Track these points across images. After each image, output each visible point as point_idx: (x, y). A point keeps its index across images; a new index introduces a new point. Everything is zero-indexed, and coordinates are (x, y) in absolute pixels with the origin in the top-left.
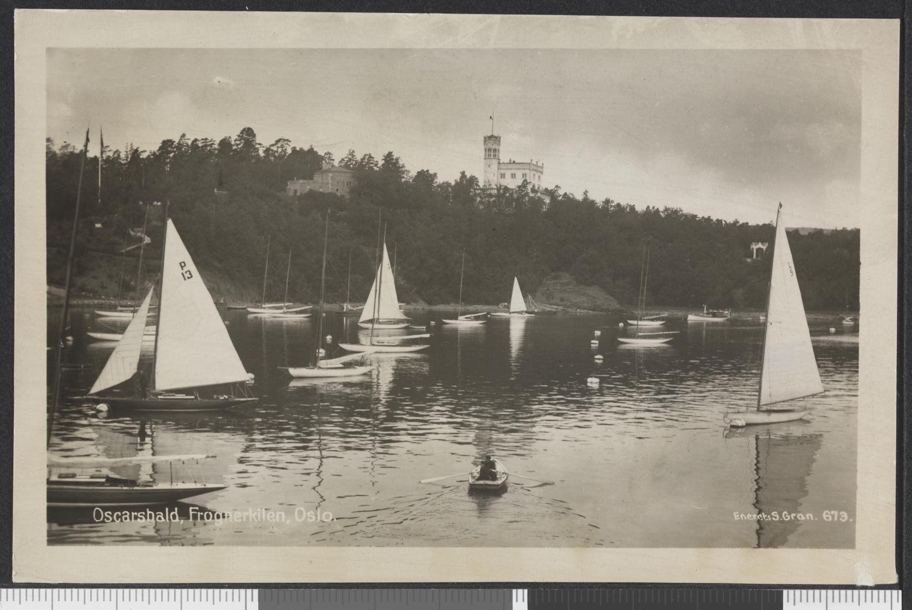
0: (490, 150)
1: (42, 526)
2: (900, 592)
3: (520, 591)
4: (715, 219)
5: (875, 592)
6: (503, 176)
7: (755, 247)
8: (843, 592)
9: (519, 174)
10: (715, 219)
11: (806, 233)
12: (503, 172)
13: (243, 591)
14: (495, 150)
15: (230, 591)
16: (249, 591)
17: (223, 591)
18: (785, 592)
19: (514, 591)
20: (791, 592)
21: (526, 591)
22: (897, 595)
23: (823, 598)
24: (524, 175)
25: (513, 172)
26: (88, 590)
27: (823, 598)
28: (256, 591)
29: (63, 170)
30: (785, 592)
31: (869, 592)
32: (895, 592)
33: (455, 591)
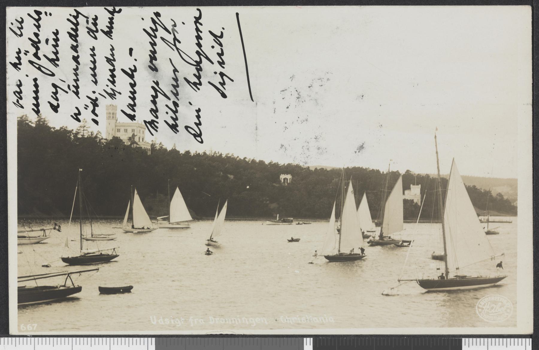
0: (110, 113)
1: (16, 304)
2: (531, 339)
3: (308, 339)
4: (257, 161)
5: (33, 339)
6: (119, 130)
7: (282, 177)
8: (512, 339)
9: (130, 130)
10: (257, 161)
11: (320, 169)
12: (119, 128)
13: (146, 339)
14: (113, 114)
15: (138, 339)
16: (150, 339)
17: (135, 339)
18: (463, 339)
19: (305, 339)
20: (467, 339)
21: (312, 339)
22: (529, 341)
23: (486, 343)
24: (133, 130)
25: (126, 128)
26: (131, 339)
27: (486, 343)
28: (154, 339)
29: (22, 291)
30: (463, 339)
31: (29, 339)
32: (528, 339)
33: (271, 339)
